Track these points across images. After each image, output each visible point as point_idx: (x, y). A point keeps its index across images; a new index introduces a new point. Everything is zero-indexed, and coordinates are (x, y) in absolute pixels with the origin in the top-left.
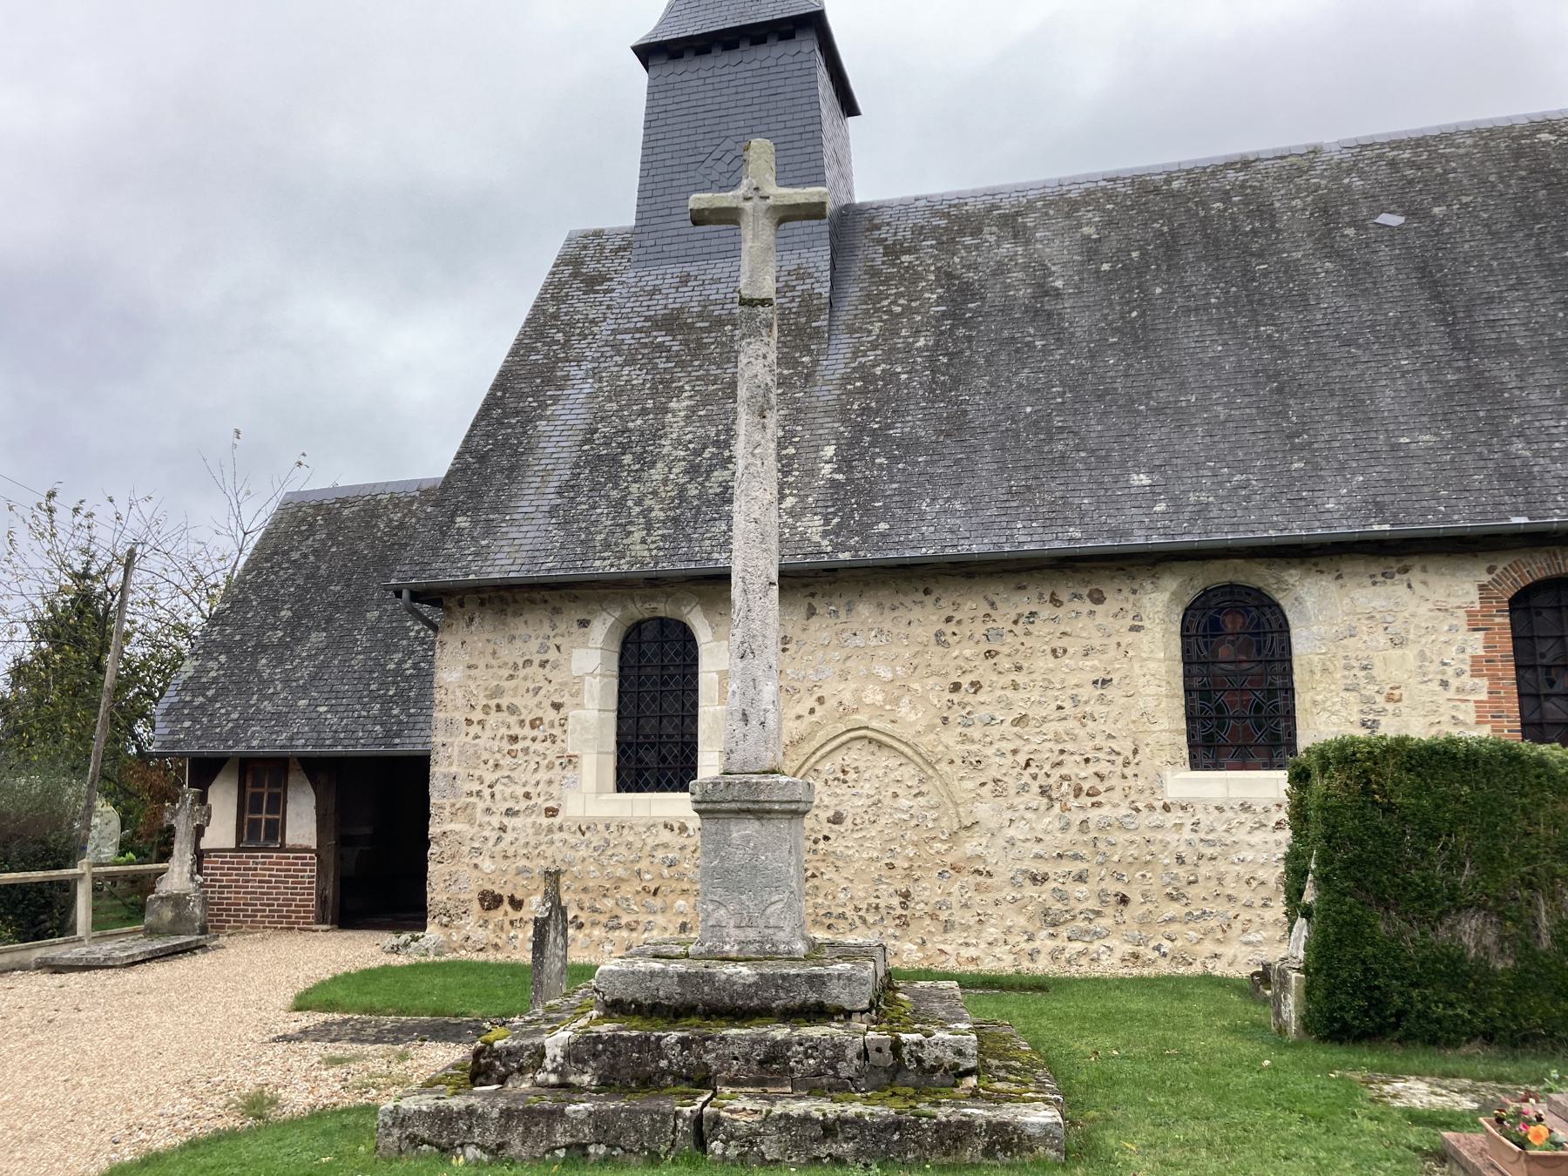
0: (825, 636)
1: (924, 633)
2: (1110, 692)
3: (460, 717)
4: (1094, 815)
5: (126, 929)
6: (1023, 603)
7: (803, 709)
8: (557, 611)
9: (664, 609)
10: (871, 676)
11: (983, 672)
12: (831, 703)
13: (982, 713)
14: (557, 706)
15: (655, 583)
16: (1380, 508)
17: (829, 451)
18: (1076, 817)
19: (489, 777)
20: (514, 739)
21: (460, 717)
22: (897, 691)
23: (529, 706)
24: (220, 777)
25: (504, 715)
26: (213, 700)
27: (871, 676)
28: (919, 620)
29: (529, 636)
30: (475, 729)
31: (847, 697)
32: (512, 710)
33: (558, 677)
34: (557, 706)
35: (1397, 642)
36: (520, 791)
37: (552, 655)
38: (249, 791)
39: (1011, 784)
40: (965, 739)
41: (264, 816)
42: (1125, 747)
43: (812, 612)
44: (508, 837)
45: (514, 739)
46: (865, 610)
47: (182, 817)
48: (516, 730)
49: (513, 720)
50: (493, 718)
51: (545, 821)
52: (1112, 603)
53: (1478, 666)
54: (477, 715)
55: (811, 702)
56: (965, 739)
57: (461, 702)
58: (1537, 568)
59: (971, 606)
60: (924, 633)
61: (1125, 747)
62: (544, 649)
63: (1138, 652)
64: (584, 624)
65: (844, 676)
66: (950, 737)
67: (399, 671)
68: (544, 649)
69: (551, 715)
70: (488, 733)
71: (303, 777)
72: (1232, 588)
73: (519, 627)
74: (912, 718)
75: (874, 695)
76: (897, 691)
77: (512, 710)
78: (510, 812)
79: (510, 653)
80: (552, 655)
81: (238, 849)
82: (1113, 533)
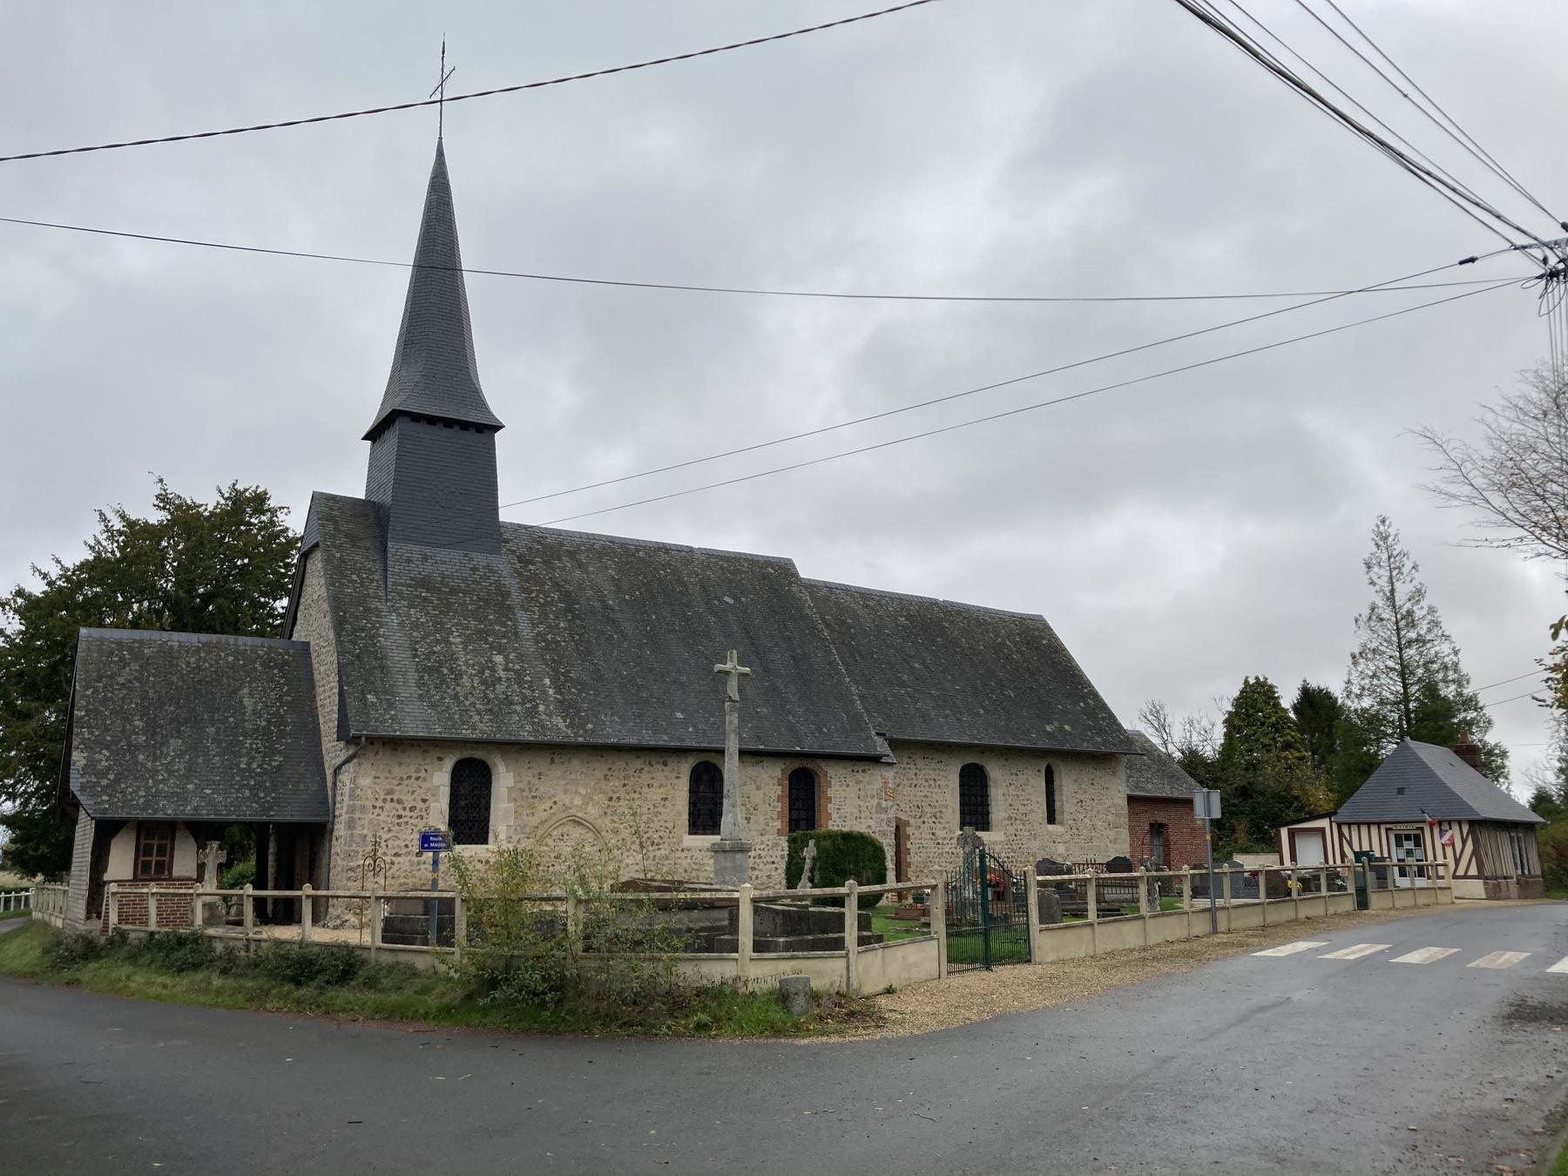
0: (559, 773)
1: (599, 774)
2: (668, 803)
3: (369, 804)
4: (658, 853)
5: (708, 895)
6: (639, 764)
7: (547, 806)
8: (426, 751)
9: (479, 755)
10: (577, 793)
11: (622, 793)
12: (560, 804)
13: (620, 810)
14: (424, 801)
15: (478, 743)
16: (759, 738)
17: (547, 681)
18: (651, 854)
19: (385, 836)
20: (400, 817)
21: (369, 804)
22: (588, 799)
23: (409, 800)
24: (178, 834)
25: (395, 805)
26: (117, 781)
27: (577, 793)
28: (600, 768)
29: (409, 765)
30: (377, 811)
31: (567, 802)
32: (400, 801)
33: (425, 785)
34: (424, 801)
35: (758, 788)
36: (402, 844)
37: (422, 774)
38: (143, 842)
39: (629, 841)
40: (613, 821)
41: (154, 859)
42: (670, 825)
43: (553, 761)
44: (396, 867)
45: (400, 817)
46: (575, 762)
47: (211, 858)
48: (401, 812)
49: (399, 807)
50: (388, 806)
51: (416, 859)
52: (669, 768)
53: (779, 799)
54: (379, 804)
55: (550, 804)
56: (613, 821)
57: (370, 796)
58: (797, 764)
59: (619, 763)
60: (599, 774)
61: (670, 825)
62: (418, 771)
63: (671, 790)
64: (440, 759)
65: (565, 792)
66: (607, 821)
67: (250, 770)
68: (418, 771)
69: (420, 805)
70: (384, 814)
71: (187, 833)
72: (706, 763)
73: (405, 758)
74: (593, 812)
75: (578, 801)
76: (588, 799)
77: (400, 801)
78: (396, 855)
79: (398, 772)
80: (422, 774)
81: (135, 879)
82: (679, 739)
